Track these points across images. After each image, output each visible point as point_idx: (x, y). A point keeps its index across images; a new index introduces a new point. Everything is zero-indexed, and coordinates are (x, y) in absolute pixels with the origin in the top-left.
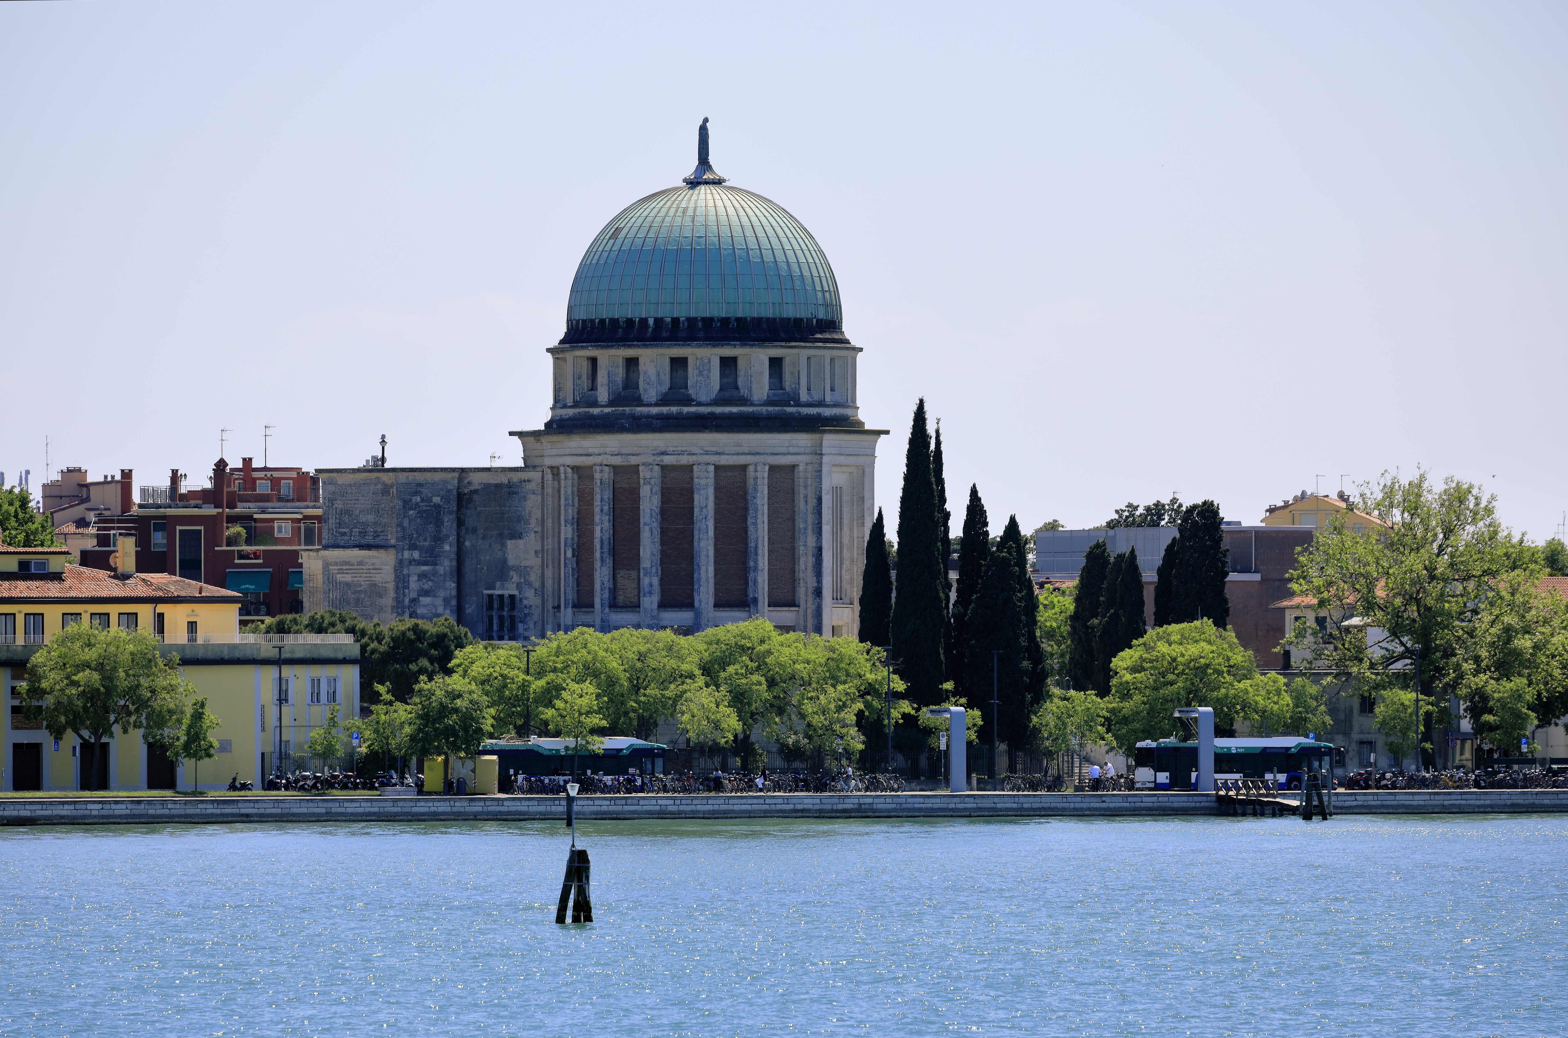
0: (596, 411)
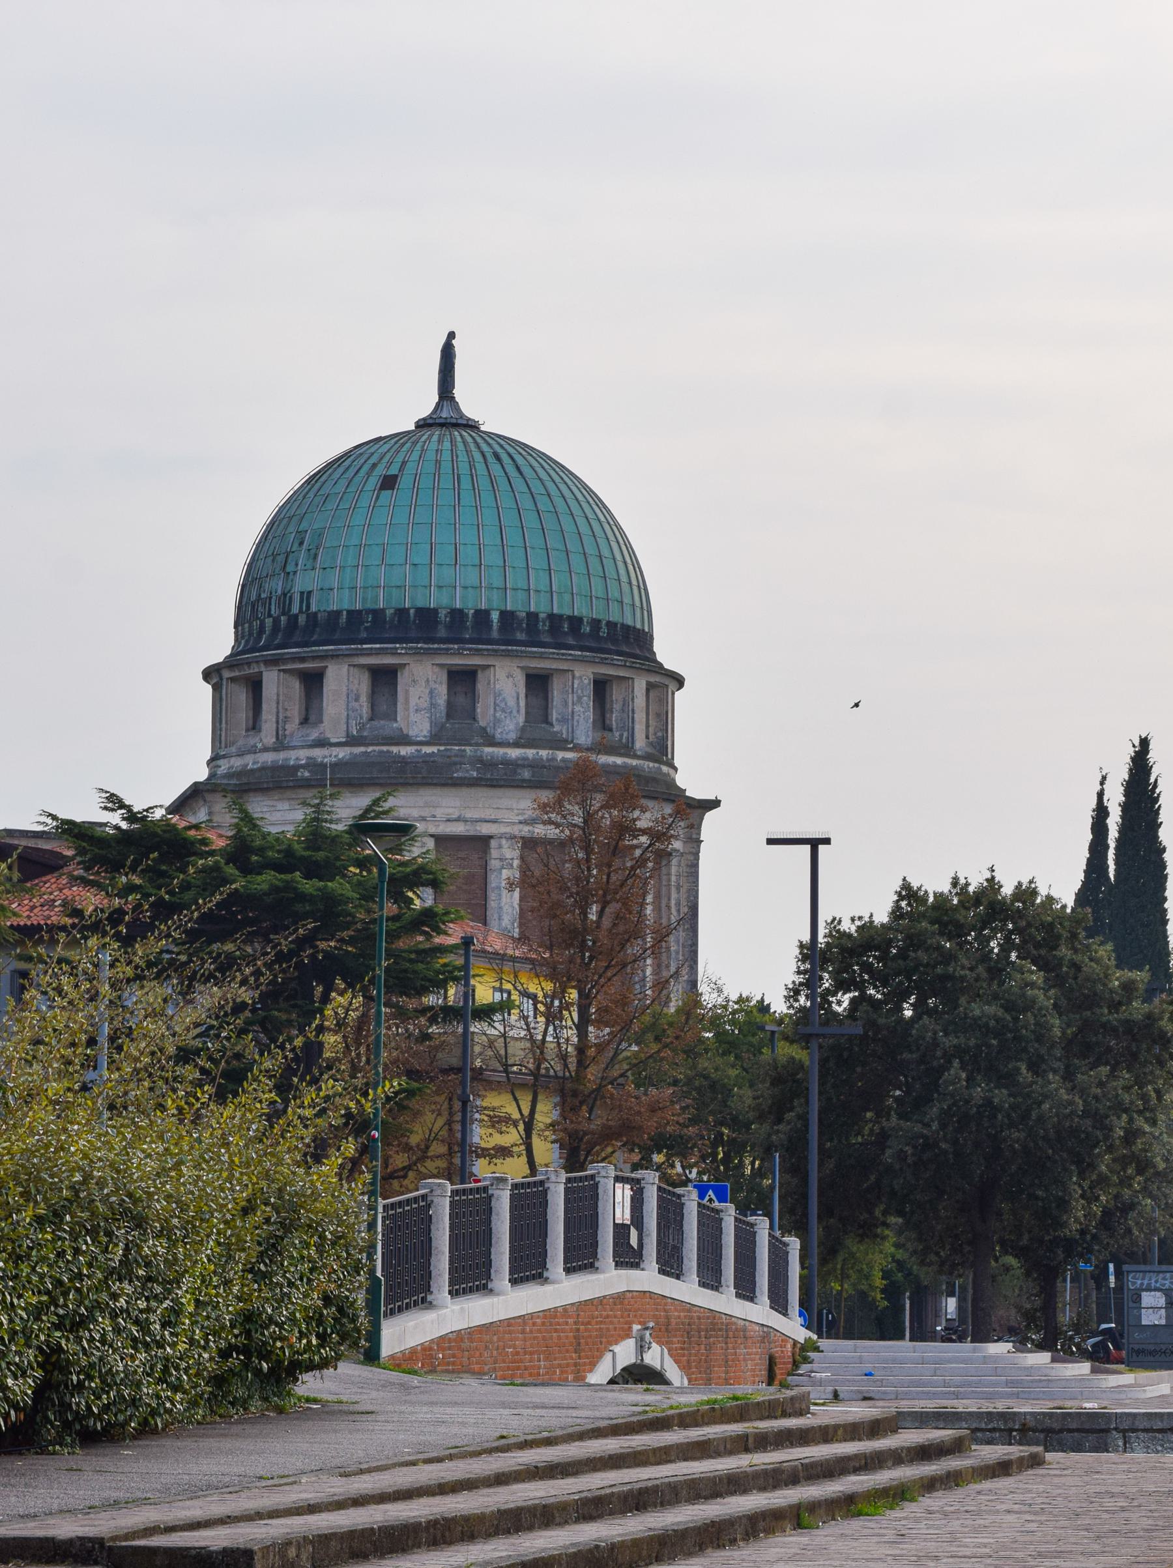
0: (405, 751)
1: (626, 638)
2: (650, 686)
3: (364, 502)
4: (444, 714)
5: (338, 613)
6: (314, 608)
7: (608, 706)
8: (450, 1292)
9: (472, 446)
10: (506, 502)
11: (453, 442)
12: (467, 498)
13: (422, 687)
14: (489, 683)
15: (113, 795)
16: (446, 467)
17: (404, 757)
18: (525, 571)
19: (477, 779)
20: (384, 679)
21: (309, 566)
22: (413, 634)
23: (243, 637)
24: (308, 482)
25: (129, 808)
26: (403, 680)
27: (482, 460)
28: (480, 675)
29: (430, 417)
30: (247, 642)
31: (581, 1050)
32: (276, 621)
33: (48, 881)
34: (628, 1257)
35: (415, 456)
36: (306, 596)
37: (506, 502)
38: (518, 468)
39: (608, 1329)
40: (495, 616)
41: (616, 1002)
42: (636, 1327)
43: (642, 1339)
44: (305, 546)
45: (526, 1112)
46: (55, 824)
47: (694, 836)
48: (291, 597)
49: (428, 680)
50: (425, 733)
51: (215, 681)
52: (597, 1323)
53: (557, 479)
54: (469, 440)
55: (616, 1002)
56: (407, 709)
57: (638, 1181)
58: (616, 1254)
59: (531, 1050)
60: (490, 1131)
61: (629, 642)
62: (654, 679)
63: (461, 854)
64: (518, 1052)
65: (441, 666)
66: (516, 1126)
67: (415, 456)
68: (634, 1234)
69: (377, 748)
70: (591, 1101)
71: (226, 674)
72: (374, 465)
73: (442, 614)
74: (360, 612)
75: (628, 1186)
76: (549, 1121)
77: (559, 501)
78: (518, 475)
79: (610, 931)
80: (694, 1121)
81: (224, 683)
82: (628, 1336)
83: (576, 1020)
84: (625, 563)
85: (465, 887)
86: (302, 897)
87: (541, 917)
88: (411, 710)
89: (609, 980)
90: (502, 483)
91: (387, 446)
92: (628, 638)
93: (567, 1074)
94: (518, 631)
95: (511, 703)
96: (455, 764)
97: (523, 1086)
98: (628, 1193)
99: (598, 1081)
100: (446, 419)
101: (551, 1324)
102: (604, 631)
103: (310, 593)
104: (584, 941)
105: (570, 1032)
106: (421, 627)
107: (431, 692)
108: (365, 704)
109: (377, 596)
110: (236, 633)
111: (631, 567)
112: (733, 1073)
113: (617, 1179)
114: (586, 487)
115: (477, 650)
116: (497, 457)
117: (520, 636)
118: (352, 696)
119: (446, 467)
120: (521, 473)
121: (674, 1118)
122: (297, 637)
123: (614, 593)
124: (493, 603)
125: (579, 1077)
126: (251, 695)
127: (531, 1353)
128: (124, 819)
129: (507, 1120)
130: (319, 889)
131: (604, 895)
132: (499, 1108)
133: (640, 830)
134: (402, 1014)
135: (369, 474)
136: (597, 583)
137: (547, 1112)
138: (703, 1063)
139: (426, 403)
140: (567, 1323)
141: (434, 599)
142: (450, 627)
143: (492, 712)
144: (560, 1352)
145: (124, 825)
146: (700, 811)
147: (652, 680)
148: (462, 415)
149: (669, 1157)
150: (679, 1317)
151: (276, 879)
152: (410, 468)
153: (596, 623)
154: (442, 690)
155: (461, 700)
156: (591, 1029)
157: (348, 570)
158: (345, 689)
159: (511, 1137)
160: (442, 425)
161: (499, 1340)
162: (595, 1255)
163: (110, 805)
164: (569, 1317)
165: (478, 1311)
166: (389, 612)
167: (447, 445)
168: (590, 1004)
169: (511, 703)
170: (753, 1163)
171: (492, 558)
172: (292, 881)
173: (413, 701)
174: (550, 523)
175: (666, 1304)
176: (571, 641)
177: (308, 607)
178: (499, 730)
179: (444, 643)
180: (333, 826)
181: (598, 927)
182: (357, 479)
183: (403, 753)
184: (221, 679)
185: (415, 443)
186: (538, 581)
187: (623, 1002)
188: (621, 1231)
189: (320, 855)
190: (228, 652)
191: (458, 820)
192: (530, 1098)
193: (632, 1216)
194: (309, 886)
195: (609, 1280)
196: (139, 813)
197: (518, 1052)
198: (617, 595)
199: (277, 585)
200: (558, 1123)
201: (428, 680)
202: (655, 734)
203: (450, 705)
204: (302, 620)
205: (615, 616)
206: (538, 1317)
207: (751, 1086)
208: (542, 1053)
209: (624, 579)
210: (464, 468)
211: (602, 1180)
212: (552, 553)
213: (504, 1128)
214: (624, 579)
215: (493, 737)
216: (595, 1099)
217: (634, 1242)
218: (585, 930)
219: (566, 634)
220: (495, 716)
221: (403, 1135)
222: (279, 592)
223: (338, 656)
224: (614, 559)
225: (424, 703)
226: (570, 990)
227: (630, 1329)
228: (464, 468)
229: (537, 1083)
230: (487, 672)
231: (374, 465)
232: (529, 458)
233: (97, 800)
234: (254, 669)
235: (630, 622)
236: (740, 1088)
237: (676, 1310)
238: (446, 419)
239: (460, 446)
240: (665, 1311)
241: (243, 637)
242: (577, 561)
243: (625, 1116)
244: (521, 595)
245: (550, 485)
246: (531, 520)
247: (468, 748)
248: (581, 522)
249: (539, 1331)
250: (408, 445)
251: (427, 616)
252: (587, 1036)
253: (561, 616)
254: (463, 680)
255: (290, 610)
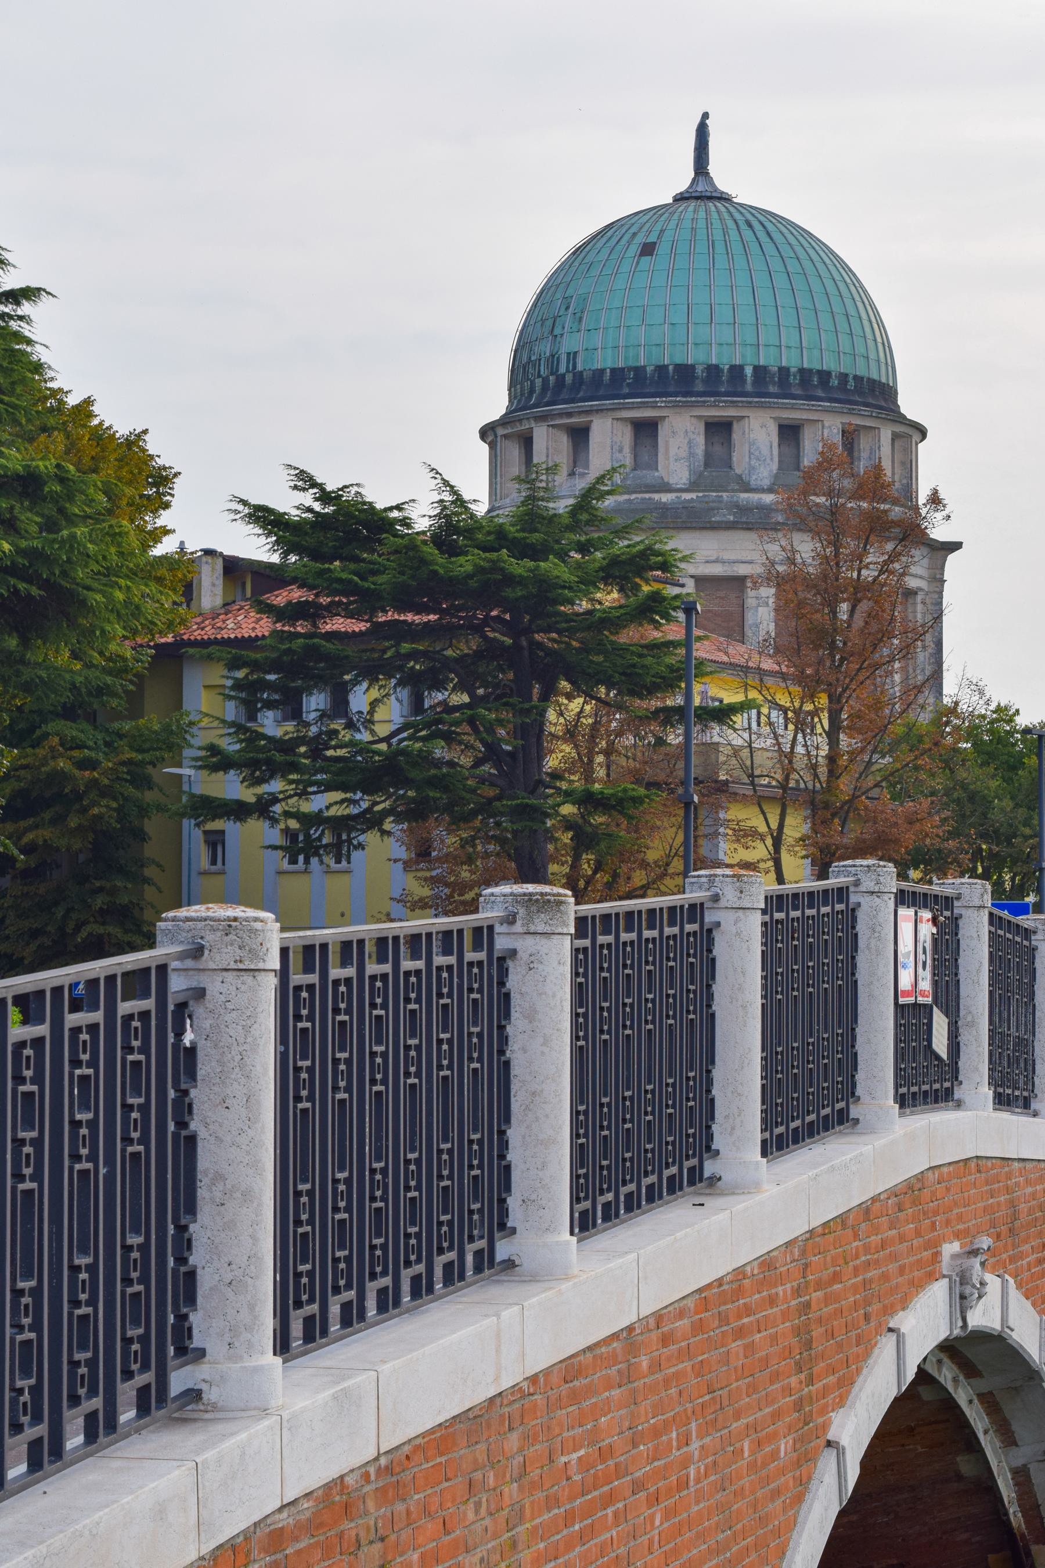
0: (666, 498)
1: (872, 390)
2: (895, 436)
3: (625, 267)
4: (702, 463)
5: (602, 371)
6: (579, 368)
7: (856, 454)
8: (282, 1346)
9: (726, 215)
10: (758, 264)
11: (707, 212)
12: (721, 262)
13: (681, 435)
14: (744, 433)
15: (302, 471)
16: (701, 234)
17: (665, 504)
18: (776, 329)
19: (734, 522)
20: (646, 431)
21: (575, 329)
22: (672, 389)
23: (515, 398)
24: (574, 253)
25: (320, 486)
26: (663, 431)
27: (735, 227)
28: (735, 426)
29: (687, 191)
30: (519, 401)
31: (832, 759)
32: (545, 381)
33: (280, 594)
34: (926, 1083)
35: (672, 224)
36: (572, 356)
37: (758, 264)
38: (768, 234)
39: (885, 1277)
40: (749, 371)
41: (869, 707)
42: (951, 1248)
43: (964, 1278)
44: (571, 310)
45: (774, 825)
46: (247, 511)
47: (938, 576)
48: (558, 358)
49: (686, 431)
50: (684, 480)
51: (490, 439)
52: (856, 1271)
53: (806, 244)
54: (723, 209)
55: (869, 707)
56: (667, 458)
57: (948, 902)
58: (901, 1077)
59: (780, 761)
60: (735, 846)
61: (876, 395)
62: (900, 429)
63: (722, 594)
64: (765, 762)
65: (699, 417)
66: (763, 841)
67: (672, 224)
68: (940, 1023)
69: (640, 496)
70: (842, 814)
71: (500, 431)
72: (634, 234)
73: (699, 370)
74: (623, 369)
75: (927, 915)
76: (798, 835)
77: (807, 264)
78: (768, 240)
79: (862, 631)
80: (953, 834)
81: (499, 439)
82: (933, 1276)
83: (827, 728)
84: (870, 321)
85: (723, 624)
86: (510, 580)
87: (787, 617)
88: (672, 459)
89: (862, 683)
90: (754, 247)
91: (647, 217)
92: (873, 391)
93: (818, 785)
94: (770, 384)
95: (765, 451)
96: (713, 509)
97: (771, 799)
98: (927, 930)
99: (851, 793)
100: (702, 192)
101: (724, 1319)
102: (851, 384)
103: (575, 353)
104: (834, 642)
105: (820, 739)
106: (679, 382)
107: (690, 442)
108: (629, 455)
109: (638, 355)
110: (510, 394)
111: (875, 326)
112: (994, 784)
113: (902, 898)
114: (832, 252)
115: (732, 402)
116: (749, 225)
117: (773, 389)
118: (616, 447)
119: (701, 234)
120: (771, 238)
121: (934, 827)
122: (564, 395)
123: (860, 349)
124: (747, 358)
125: (830, 788)
126: (523, 451)
127: (656, 1433)
128: (316, 499)
129: (754, 833)
130: (530, 570)
131: (855, 594)
132: (743, 821)
133: (893, 522)
134: (636, 722)
135: (629, 243)
136: (844, 339)
137: (796, 826)
138: (962, 774)
139: (683, 178)
140: (772, 1301)
141: (695, 357)
142: (706, 381)
143: (747, 460)
144: (752, 1389)
145: (317, 506)
146: (943, 553)
147: (897, 430)
148: (716, 190)
149: (926, 873)
150: (1034, 1196)
151: (480, 558)
152: (668, 235)
153: (844, 377)
154: (700, 440)
155: (718, 450)
156: (842, 736)
157: (611, 331)
158: (609, 441)
159: (759, 851)
160: (697, 198)
161: (530, 1439)
162: (850, 1092)
163: (300, 483)
164: (781, 1280)
165: (436, 1363)
166: (649, 369)
167: (702, 214)
168: (841, 709)
169: (765, 451)
170: (1013, 879)
171: (746, 316)
172: (499, 560)
173: (673, 451)
174: (799, 283)
175: (1009, 1176)
176: (820, 393)
177: (574, 367)
178: (754, 477)
179: (701, 396)
180: (551, 505)
181: (849, 626)
182: (619, 247)
183: (664, 500)
184: (496, 437)
185: (673, 214)
186: (789, 337)
187: (877, 706)
188: (912, 1019)
189: (536, 537)
190: (504, 411)
191: (716, 561)
192: (778, 811)
193: (935, 984)
194: (519, 567)
195: (889, 1147)
196: (333, 492)
197: (765, 762)
198: (863, 351)
199: (545, 348)
200: (809, 838)
201: (686, 431)
202: (900, 481)
203: (708, 455)
204: (569, 378)
205: (861, 371)
206: (681, 1314)
207: (1012, 798)
208: (790, 762)
209: (869, 335)
210: (718, 235)
211: (865, 901)
212: (802, 312)
213: (750, 843)
214: (869, 335)
215: (749, 484)
216: (848, 812)
217: (940, 1044)
218: (835, 630)
219: (816, 386)
220: (750, 464)
221: (639, 852)
222: (548, 354)
223: (602, 410)
224: (860, 318)
225: (683, 453)
226: (820, 695)
227: (936, 1256)
228: (718, 235)
229: (785, 797)
230: (742, 423)
231: (634, 234)
232: (779, 225)
233: (284, 479)
234: (526, 425)
235: (875, 376)
236: (1000, 800)
237: (1028, 1183)
238: (702, 192)
239: (715, 215)
240: (1008, 1190)
241: (515, 398)
242: (825, 320)
243: (880, 829)
244: (773, 350)
245: (798, 249)
246: (781, 281)
247: (725, 495)
248: (829, 283)
249: (687, 1353)
250: (666, 215)
251: (685, 372)
252: (838, 744)
253: (810, 371)
254: (719, 431)
255: (557, 370)
